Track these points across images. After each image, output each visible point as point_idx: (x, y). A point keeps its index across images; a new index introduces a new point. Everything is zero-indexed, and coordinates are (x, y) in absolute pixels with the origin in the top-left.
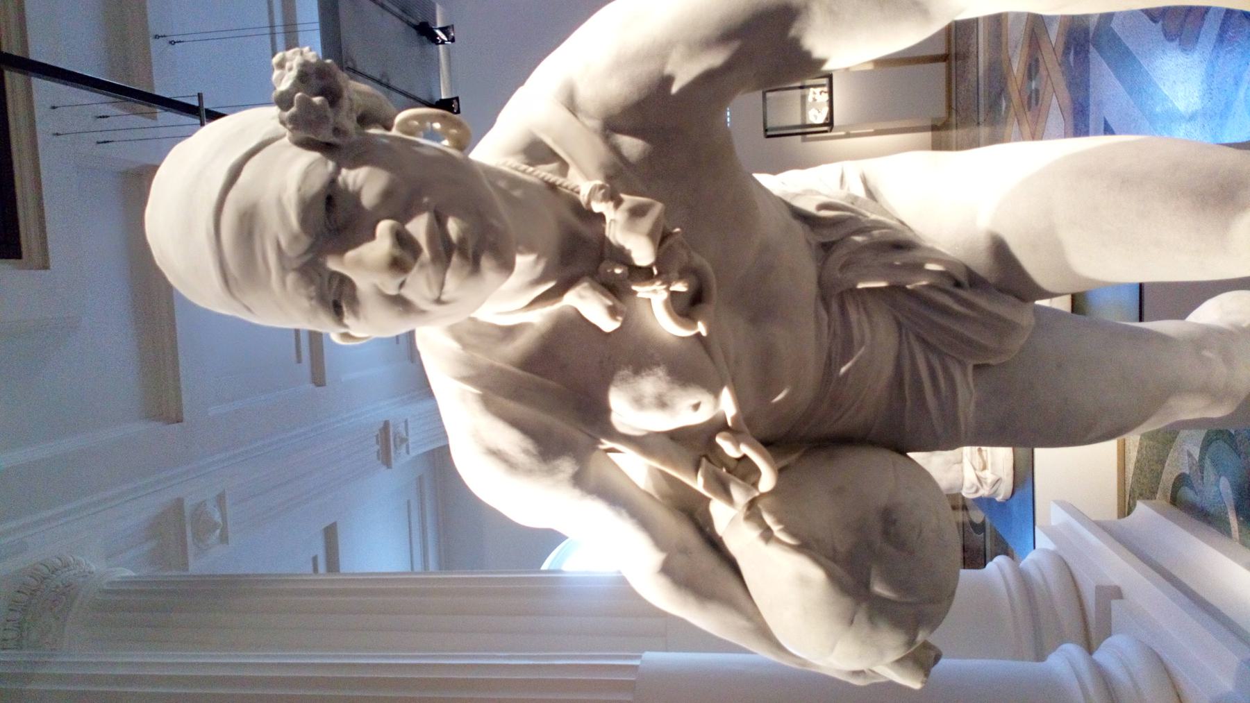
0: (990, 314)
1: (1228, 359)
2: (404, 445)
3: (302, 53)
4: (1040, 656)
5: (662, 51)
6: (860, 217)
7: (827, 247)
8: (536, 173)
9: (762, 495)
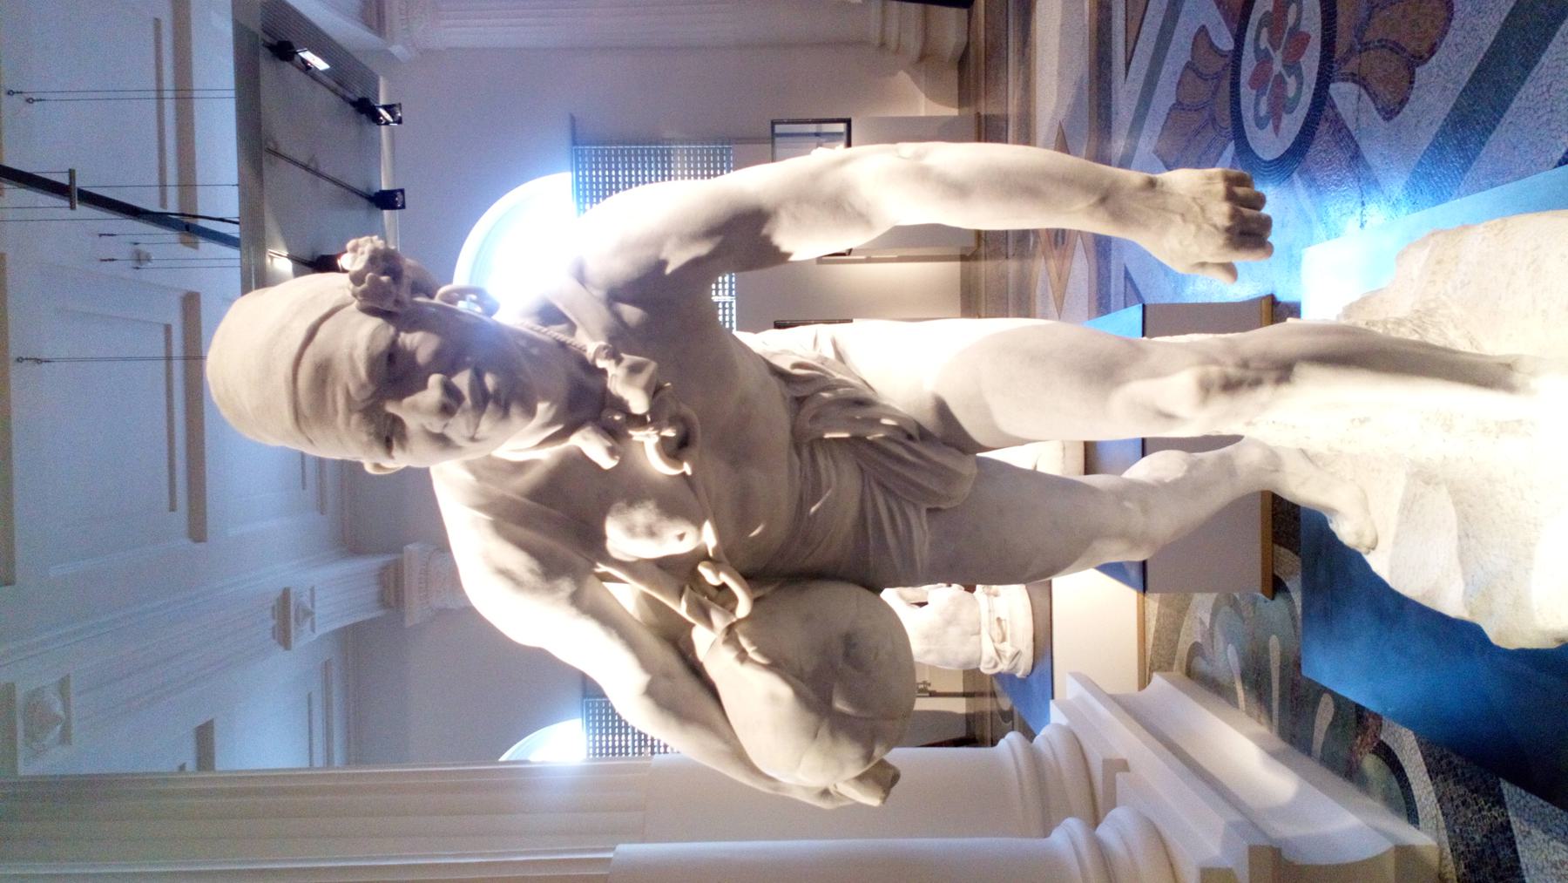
0: (935, 463)
2: (309, 620)
3: (372, 241)
5: (659, 241)
6: (828, 376)
7: (800, 401)
8: (549, 333)
9: (740, 621)
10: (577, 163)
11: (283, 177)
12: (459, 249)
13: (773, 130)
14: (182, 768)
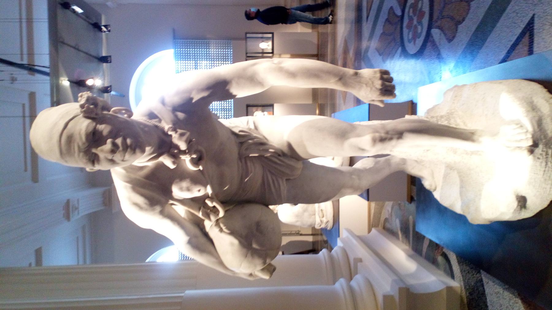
1: (359, 179)
4: (334, 284)
5: (190, 91)
7: (241, 143)
9: (220, 218)
10: (175, 46)
11: (66, 52)
12: (133, 75)
13: (246, 35)
14: (30, 265)
